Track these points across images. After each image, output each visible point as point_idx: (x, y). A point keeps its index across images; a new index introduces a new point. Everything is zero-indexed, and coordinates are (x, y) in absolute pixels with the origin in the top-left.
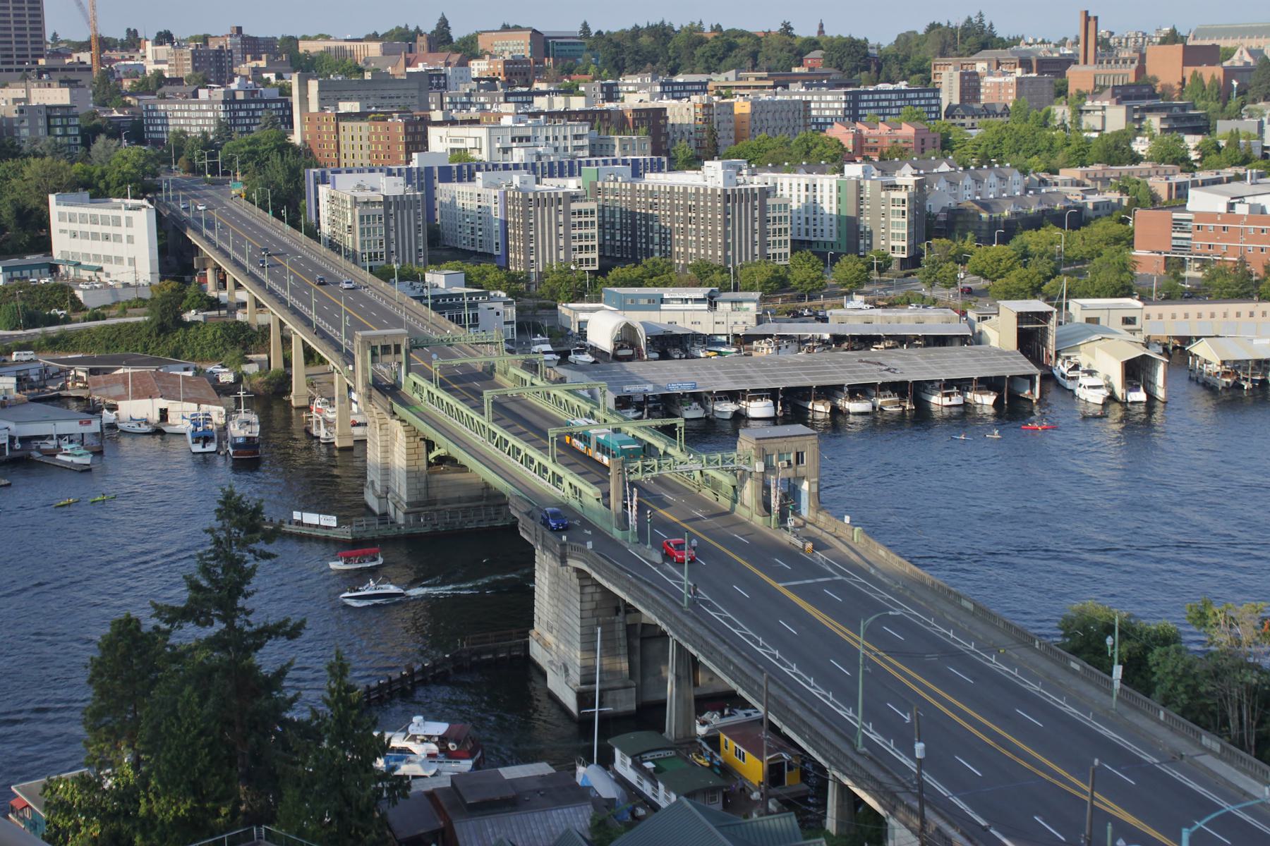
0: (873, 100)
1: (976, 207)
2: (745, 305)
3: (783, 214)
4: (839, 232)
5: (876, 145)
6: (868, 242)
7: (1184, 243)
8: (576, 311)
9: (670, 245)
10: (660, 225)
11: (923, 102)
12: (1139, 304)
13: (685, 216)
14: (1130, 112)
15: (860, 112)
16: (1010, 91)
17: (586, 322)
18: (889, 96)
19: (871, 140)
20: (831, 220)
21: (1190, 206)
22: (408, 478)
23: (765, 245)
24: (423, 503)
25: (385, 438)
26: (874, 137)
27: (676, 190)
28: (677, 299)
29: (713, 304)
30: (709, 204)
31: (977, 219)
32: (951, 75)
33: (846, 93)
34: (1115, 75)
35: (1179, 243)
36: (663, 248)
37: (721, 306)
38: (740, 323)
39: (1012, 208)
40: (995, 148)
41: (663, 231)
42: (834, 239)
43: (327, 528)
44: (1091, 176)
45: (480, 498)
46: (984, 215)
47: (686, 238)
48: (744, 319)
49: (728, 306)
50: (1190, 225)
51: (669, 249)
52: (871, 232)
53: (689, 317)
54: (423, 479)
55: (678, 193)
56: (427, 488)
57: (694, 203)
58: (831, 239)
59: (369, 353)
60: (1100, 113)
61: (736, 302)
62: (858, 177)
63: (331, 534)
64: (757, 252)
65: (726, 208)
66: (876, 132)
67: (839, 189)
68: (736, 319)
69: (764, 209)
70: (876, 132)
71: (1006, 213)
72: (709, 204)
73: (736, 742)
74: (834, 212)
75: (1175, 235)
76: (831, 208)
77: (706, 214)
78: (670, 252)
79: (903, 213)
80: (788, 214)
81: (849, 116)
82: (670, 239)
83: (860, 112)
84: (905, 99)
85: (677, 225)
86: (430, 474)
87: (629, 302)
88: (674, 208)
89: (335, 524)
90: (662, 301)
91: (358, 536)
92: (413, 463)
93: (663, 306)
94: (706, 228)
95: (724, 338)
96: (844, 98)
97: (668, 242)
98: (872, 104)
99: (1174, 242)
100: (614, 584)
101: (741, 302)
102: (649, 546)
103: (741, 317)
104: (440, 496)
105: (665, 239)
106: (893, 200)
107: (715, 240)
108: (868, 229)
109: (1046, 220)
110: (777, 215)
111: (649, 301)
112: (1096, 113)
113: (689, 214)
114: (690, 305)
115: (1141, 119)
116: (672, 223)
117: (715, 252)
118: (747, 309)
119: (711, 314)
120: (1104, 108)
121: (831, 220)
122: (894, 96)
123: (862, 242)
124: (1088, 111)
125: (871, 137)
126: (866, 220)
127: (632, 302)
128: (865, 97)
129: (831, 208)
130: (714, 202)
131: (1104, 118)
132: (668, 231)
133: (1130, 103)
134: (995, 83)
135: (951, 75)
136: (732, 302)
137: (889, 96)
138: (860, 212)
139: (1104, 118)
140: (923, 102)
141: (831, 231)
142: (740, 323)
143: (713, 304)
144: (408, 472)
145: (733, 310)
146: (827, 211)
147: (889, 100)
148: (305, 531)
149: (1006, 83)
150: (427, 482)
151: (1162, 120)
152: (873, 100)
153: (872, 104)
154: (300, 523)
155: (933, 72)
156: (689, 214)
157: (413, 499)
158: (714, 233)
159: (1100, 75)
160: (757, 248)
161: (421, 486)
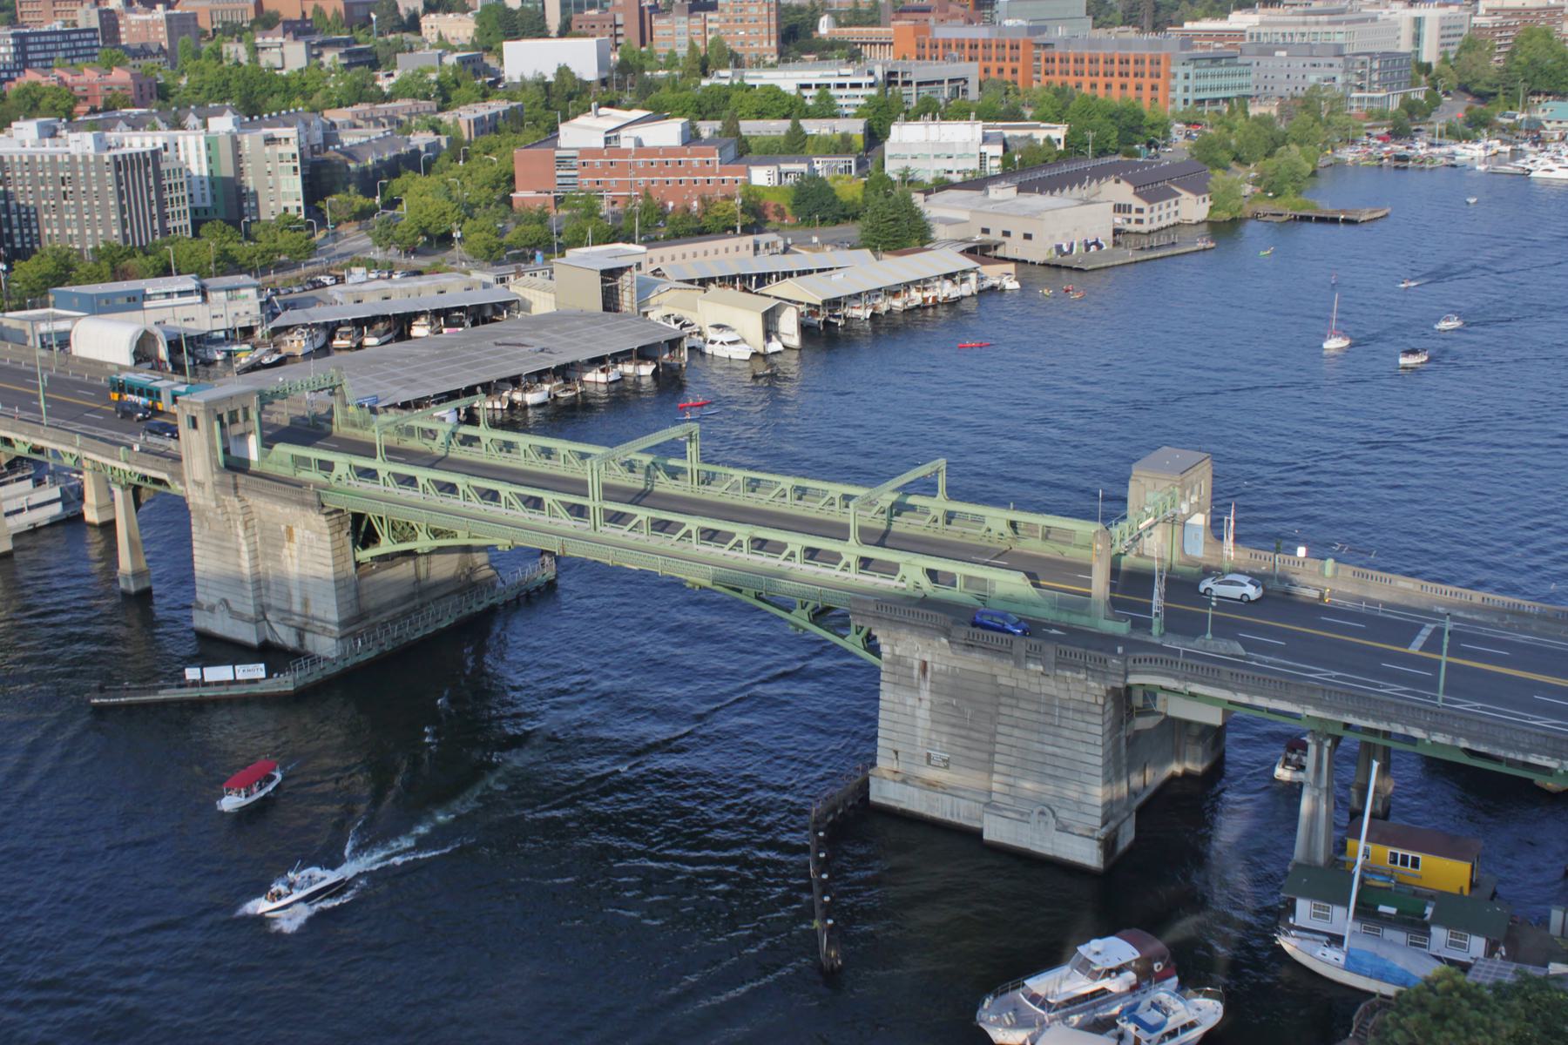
0: (39, 43)
1: (342, 157)
2: (243, 292)
3: (178, 180)
4: (214, 197)
5: (85, 94)
6: (253, 204)
7: (570, 181)
8: (35, 321)
9: (38, 227)
10: (18, 206)
11: (85, 44)
12: (642, 249)
13: (56, 191)
14: (310, 47)
15: (29, 57)
16: (160, 29)
17: (68, 333)
18: (54, 38)
19: (78, 89)
20: (202, 182)
21: (563, 141)
22: (337, 590)
23: (164, 217)
24: (356, 621)
25: (252, 539)
26: (83, 84)
27: (39, 159)
28: (160, 294)
29: (203, 292)
30: (93, 174)
31: (344, 170)
32: (87, 13)
33: (13, 36)
34: (232, 11)
35: (565, 180)
36: (26, 231)
37: (212, 296)
38: (242, 314)
39: (375, 158)
40: (220, 91)
41: (23, 210)
42: (208, 203)
43: (255, 681)
44: (361, 116)
45: (411, 597)
46: (352, 165)
47: (61, 217)
48: (247, 309)
49: (223, 295)
50: (575, 162)
51: (35, 231)
52: (255, 194)
53: (182, 313)
54: (353, 587)
55: (43, 162)
56: (358, 597)
57: (68, 174)
58: (204, 205)
59: (217, 425)
60: (277, 50)
61: (231, 289)
62: (230, 132)
63: (256, 689)
64: (156, 226)
65: (118, 178)
66: (82, 79)
67: (208, 147)
68: (236, 309)
69: (158, 176)
70: (82, 79)
71: (370, 162)
72: (93, 174)
73: (1389, 844)
74: (205, 173)
75: (559, 173)
76: (200, 169)
77: (89, 185)
78: (38, 235)
79: (295, 169)
80: (184, 179)
81: (19, 62)
82: (37, 220)
83: (29, 57)
84: (69, 41)
85: (44, 202)
86: (360, 578)
87: (103, 303)
88: (36, 182)
89: (262, 674)
90: (146, 297)
91: (301, 683)
92: (340, 568)
93: (147, 304)
94: (90, 204)
95: (222, 334)
96: (11, 41)
97: (34, 224)
98: (39, 47)
99: (559, 181)
100: (1282, 698)
101: (237, 289)
102: (1209, 636)
103: (241, 307)
104: (372, 604)
105: (28, 220)
106: (281, 155)
107: (107, 216)
108: (251, 190)
109: (402, 167)
110: (173, 181)
111: (129, 300)
112: (274, 50)
113: (63, 188)
114: (176, 300)
115: (319, 55)
116: (37, 199)
117: (108, 230)
118: (247, 296)
119: (206, 308)
120: (282, 45)
121: (202, 182)
122: (59, 38)
123: (245, 205)
124: (264, 48)
125: (78, 84)
126: (250, 182)
127: (107, 302)
128: (32, 39)
129: (200, 169)
130: (99, 171)
131: (283, 54)
132: (32, 211)
133: (308, 38)
134: (141, 21)
135: (87, 13)
136: (227, 290)
137: (54, 38)
138: (239, 171)
139: (283, 54)
140: (85, 44)
141: (203, 195)
142: (242, 314)
143: (203, 292)
144: (336, 581)
145: (231, 299)
146: (195, 172)
147: (55, 42)
148: (208, 693)
149: (155, 22)
150: (357, 590)
151: (341, 55)
152: (39, 43)
153: (39, 47)
154: (202, 683)
155: (19, 10)
156: (63, 188)
157: (345, 617)
158: (104, 209)
159: (217, 10)
160: (156, 223)
161: (351, 596)
